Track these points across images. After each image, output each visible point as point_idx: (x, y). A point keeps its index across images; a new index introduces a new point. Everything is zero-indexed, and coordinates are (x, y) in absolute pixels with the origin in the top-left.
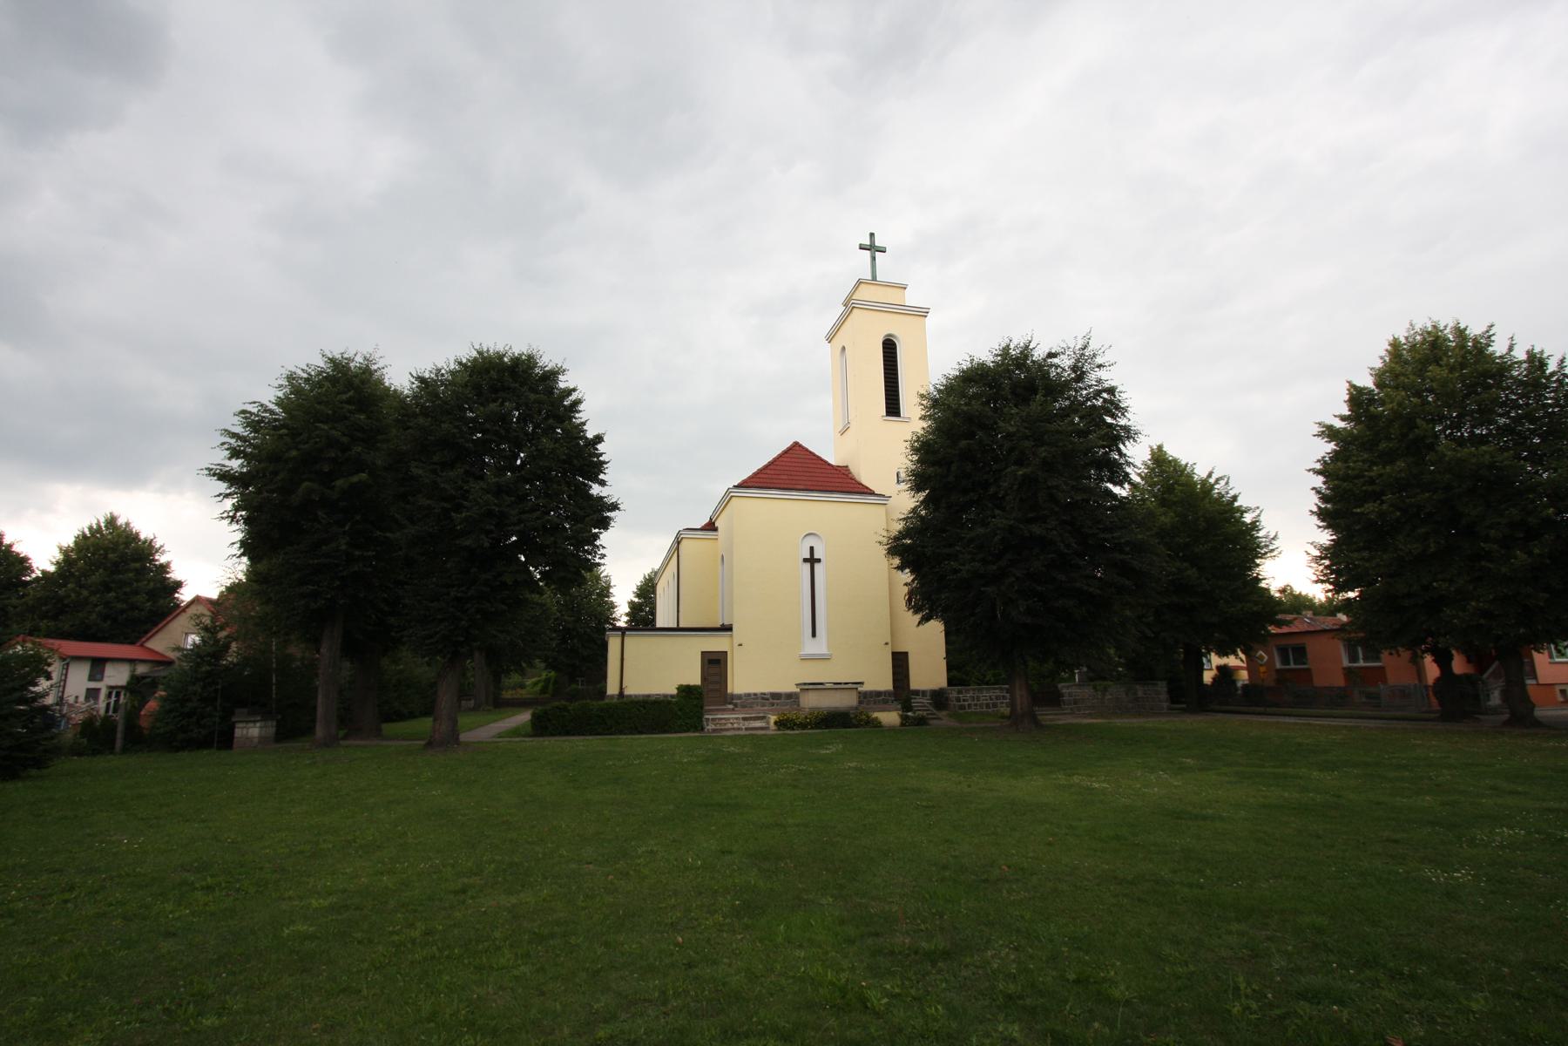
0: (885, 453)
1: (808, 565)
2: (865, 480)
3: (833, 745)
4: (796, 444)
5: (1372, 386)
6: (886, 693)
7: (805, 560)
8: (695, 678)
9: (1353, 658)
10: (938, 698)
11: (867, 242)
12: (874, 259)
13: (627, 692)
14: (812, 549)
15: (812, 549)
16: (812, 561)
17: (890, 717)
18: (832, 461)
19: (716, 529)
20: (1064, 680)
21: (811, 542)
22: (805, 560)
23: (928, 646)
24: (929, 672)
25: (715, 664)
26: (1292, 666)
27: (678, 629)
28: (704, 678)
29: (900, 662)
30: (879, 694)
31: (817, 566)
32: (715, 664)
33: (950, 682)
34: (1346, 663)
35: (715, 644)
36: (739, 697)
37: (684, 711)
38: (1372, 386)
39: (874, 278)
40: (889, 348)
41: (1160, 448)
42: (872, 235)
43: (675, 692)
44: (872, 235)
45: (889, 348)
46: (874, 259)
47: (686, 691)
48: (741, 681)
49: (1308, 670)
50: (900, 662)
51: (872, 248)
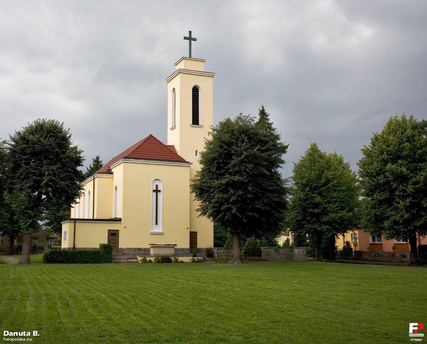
0: (191, 143)
1: (155, 193)
2: (187, 160)
3: (165, 268)
4: (151, 136)
5: (355, 169)
6: (187, 249)
7: (154, 191)
8: (106, 242)
9: (374, 240)
10: (209, 253)
11: (188, 36)
12: (190, 44)
13: (76, 247)
14: (157, 186)
15: (157, 186)
16: (157, 191)
17: (187, 259)
18: (179, 154)
19: (112, 173)
20: (321, 219)
21: (157, 183)
22: (154, 191)
23: (206, 230)
24: (206, 241)
25: (113, 235)
26: (376, 242)
27: (93, 220)
28: (109, 241)
29: (193, 236)
30: (183, 249)
31: (159, 194)
32: (113, 235)
33: (215, 245)
34: (371, 242)
35: (114, 226)
36: (124, 249)
37: (107, 254)
38: (355, 169)
39: (190, 57)
40: (196, 91)
41: (315, 145)
42: (190, 32)
43: (98, 247)
44: (190, 32)
45: (196, 91)
46: (190, 44)
47: (103, 247)
48: (124, 243)
49: (382, 244)
50: (193, 236)
51: (190, 39)
